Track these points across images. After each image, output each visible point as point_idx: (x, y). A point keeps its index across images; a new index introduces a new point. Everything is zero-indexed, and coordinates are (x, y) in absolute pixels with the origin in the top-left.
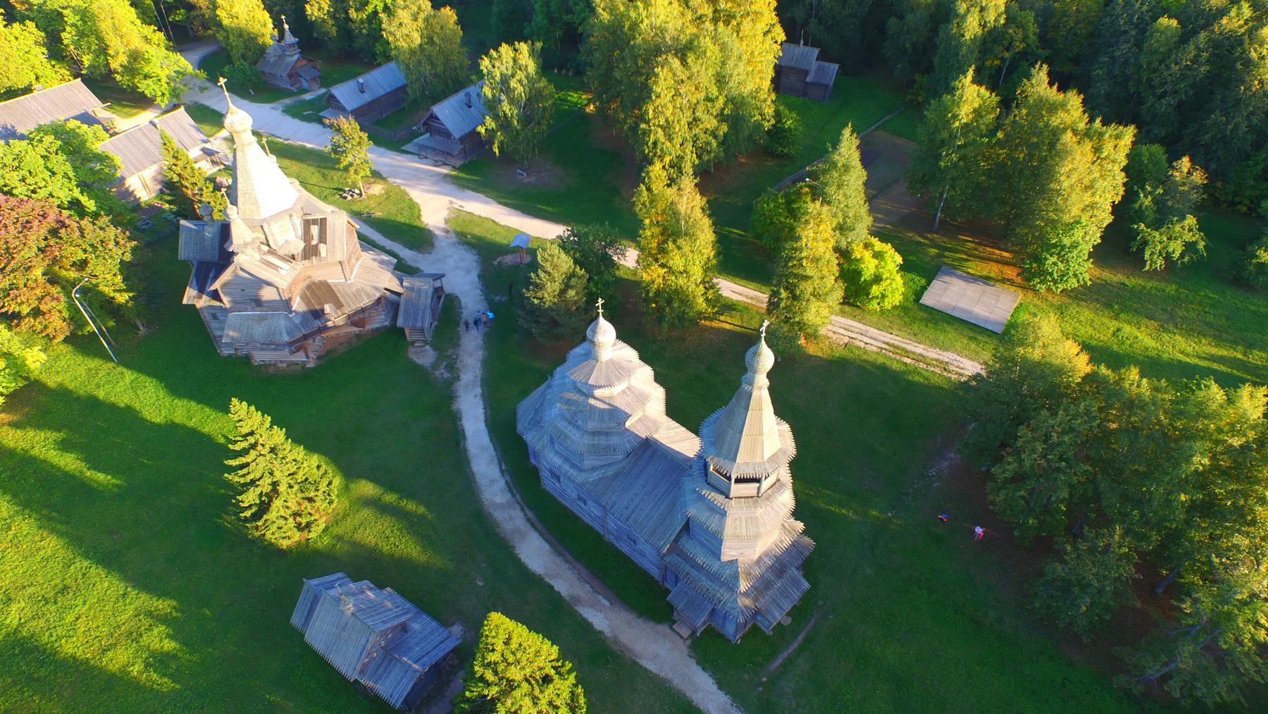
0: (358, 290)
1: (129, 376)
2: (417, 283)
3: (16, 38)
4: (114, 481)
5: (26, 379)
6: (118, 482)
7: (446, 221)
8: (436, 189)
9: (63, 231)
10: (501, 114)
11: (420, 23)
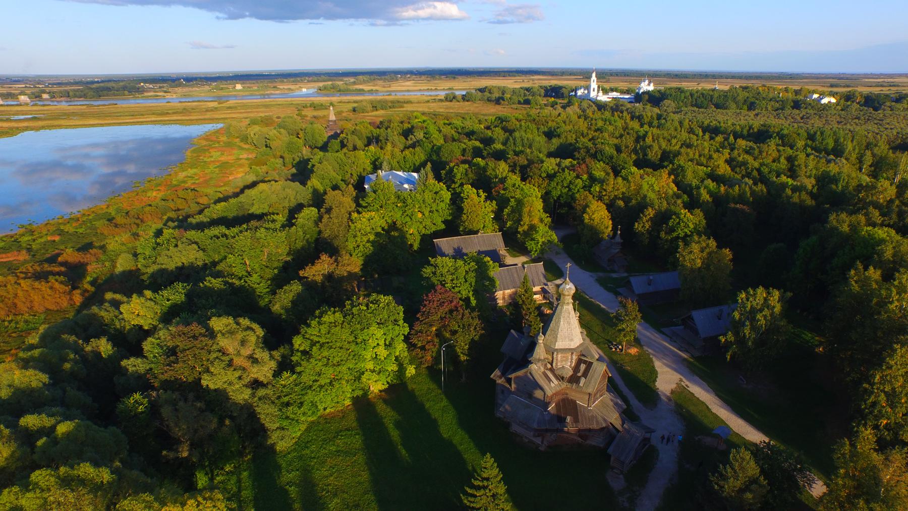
0: (593, 416)
1: (445, 402)
2: (634, 429)
3: (485, 207)
4: (408, 458)
5: (402, 380)
6: (409, 461)
7: (672, 392)
8: (674, 366)
9: (455, 313)
10: (741, 334)
11: (705, 254)
